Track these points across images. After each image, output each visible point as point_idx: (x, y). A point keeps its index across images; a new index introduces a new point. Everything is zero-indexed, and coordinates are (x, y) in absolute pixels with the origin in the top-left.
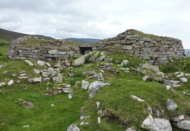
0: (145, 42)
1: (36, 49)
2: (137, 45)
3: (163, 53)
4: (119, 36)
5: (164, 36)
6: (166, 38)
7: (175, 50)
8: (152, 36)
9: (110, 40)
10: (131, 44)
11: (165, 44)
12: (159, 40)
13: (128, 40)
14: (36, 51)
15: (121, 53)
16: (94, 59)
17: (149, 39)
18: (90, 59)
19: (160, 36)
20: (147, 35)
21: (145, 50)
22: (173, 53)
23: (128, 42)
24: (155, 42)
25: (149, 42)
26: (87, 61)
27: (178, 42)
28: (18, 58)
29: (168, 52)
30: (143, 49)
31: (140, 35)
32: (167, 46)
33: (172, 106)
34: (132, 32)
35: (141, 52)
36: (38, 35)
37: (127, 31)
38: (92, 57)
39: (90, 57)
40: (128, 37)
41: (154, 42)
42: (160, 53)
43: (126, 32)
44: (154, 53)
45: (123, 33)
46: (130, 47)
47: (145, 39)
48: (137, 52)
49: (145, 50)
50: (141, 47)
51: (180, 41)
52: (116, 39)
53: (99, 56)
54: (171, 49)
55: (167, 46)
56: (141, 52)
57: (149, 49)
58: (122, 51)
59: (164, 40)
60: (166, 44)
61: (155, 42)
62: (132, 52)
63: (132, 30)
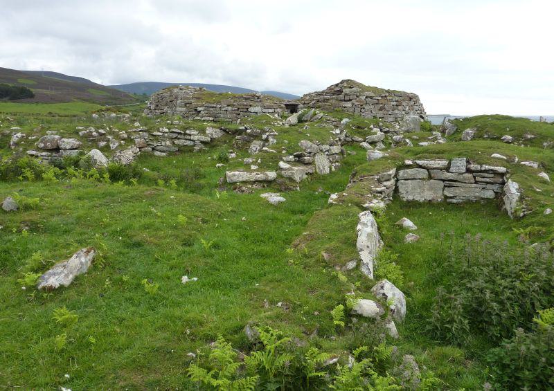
0: (366, 97)
1: (228, 106)
2: (357, 101)
3: (390, 113)
4: (330, 88)
5: (391, 89)
6: (394, 92)
7: (407, 109)
8: (375, 90)
9: (319, 94)
10: (350, 100)
11: (391, 100)
12: (383, 95)
13: (346, 94)
14: (230, 108)
15: (339, 111)
16: (309, 118)
17: (372, 94)
18: (304, 118)
19: (387, 89)
20: (369, 89)
21: (367, 107)
22: (404, 112)
23: (347, 98)
24: (379, 98)
25: (371, 98)
26: (300, 121)
27: (412, 99)
28: (198, 118)
29: (396, 112)
30: (364, 106)
31: (360, 88)
32: (395, 103)
33: (381, 124)
34: (350, 83)
35: (362, 110)
36: (45, 70)
37: (342, 82)
38: (306, 116)
39: (303, 115)
40: (347, 91)
41: (377, 98)
42: (385, 112)
43: (341, 83)
44: (378, 112)
45: (337, 85)
46: (349, 104)
47: (367, 93)
48: (358, 110)
49: (367, 107)
50: (362, 104)
51: (416, 97)
52: (327, 93)
53: (315, 114)
54: (400, 108)
55: (395, 103)
56: (362, 110)
57: (372, 107)
58: (340, 109)
59: (391, 96)
60: (394, 100)
61: (379, 98)
62: (352, 110)
63: (348, 80)
